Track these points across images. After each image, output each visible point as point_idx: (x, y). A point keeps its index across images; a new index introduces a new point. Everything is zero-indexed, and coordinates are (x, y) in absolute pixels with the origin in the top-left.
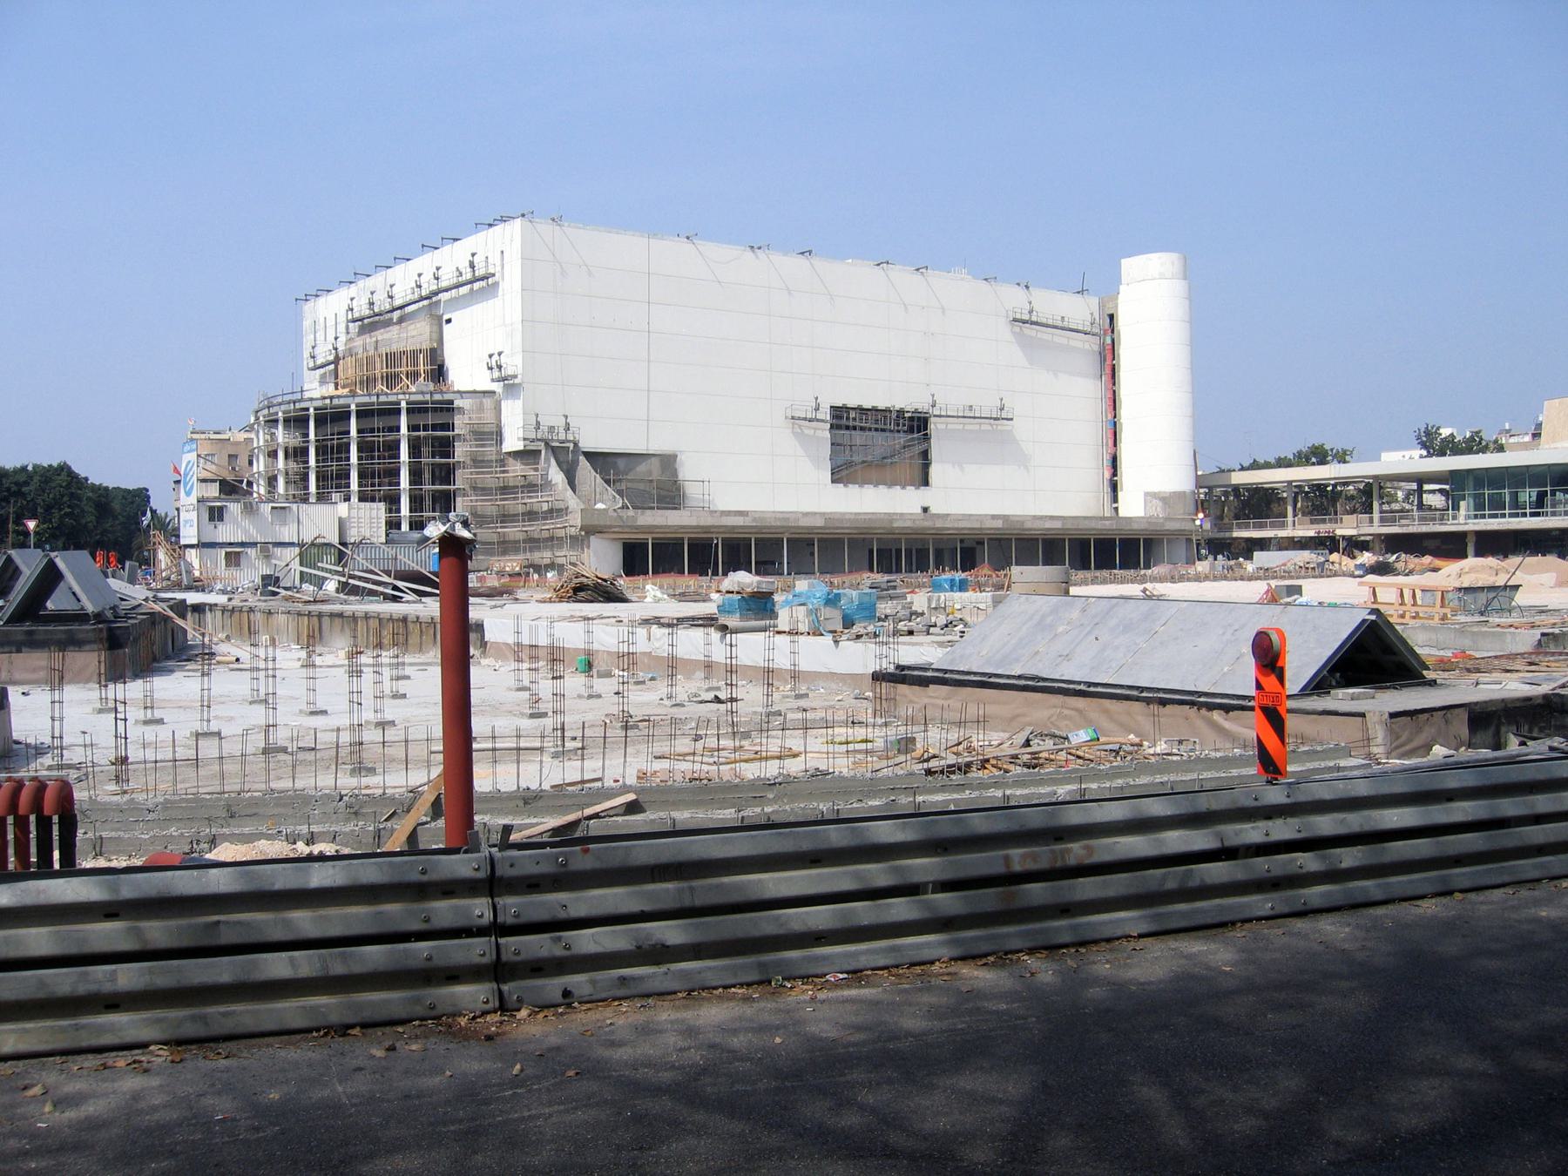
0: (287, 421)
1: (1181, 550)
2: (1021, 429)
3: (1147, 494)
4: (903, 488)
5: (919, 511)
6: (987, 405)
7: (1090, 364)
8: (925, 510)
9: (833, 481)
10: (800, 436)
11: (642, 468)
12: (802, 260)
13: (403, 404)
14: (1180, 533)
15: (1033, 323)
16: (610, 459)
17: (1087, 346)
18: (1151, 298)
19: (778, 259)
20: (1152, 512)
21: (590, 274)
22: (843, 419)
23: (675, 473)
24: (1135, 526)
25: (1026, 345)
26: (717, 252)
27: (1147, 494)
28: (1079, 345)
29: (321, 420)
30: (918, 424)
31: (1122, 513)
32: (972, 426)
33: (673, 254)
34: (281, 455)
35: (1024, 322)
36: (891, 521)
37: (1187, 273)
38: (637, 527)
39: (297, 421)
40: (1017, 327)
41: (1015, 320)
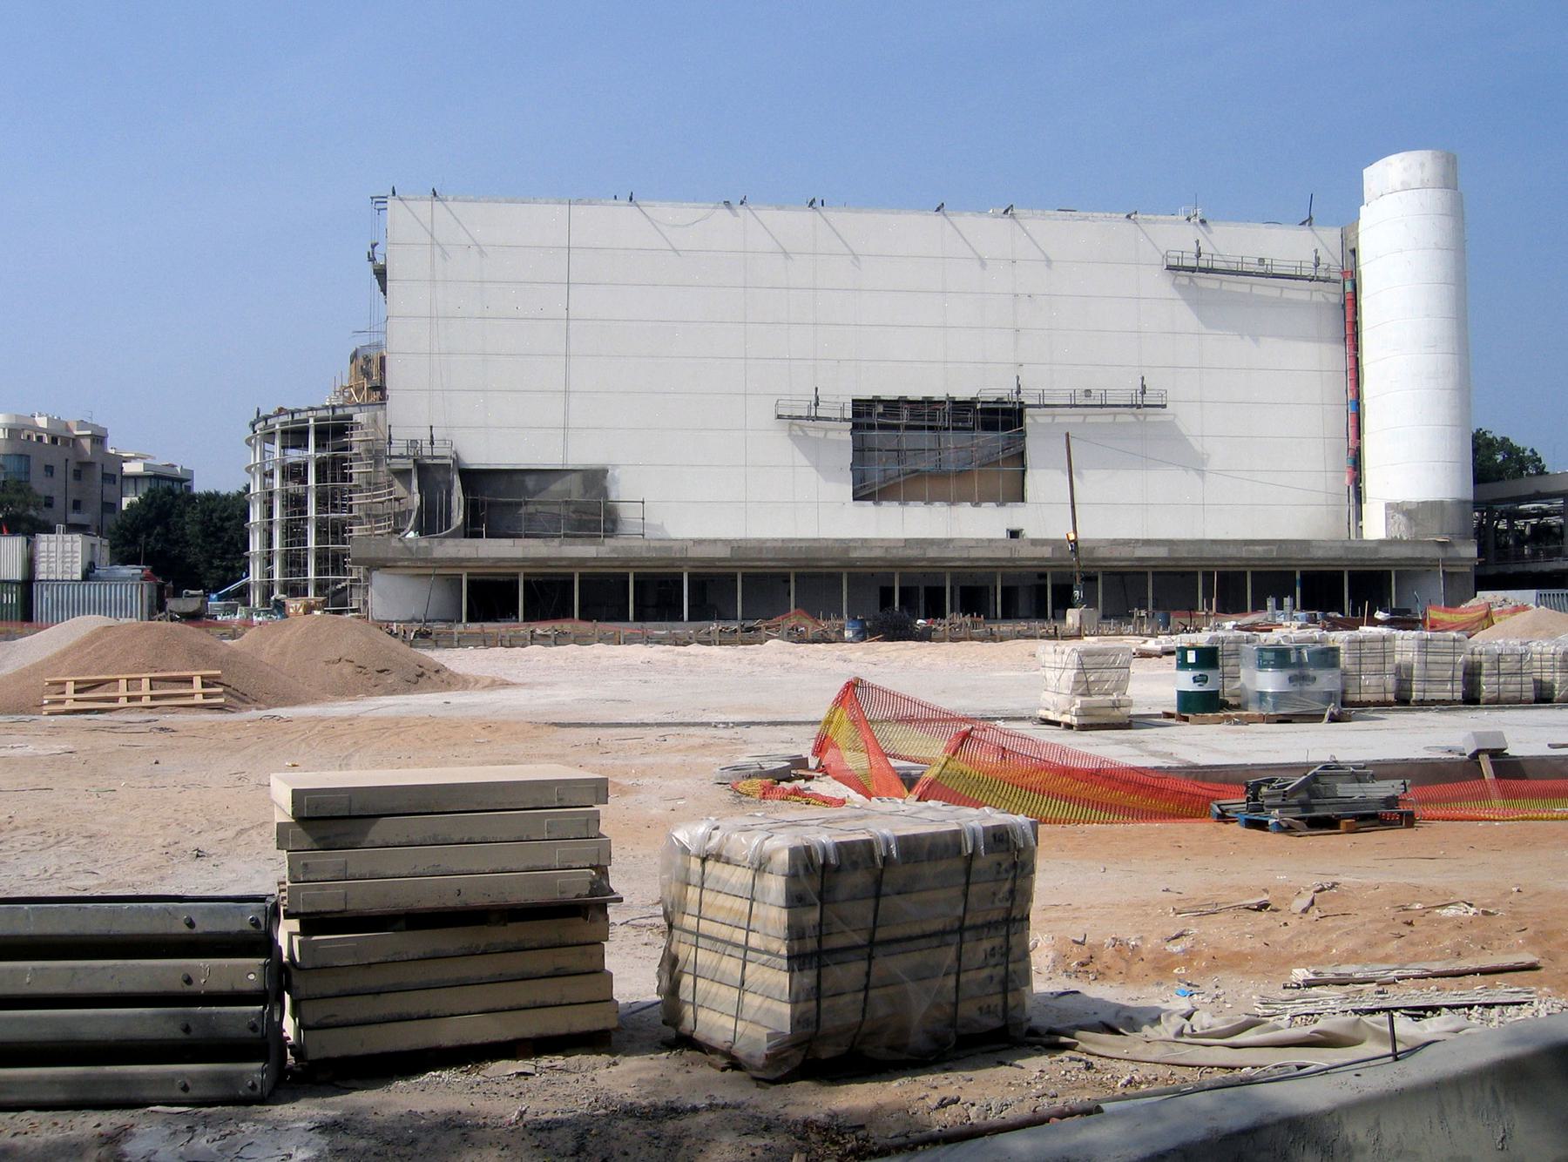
0: (284, 432)
1: (1437, 587)
2: (1186, 417)
3: (1389, 506)
4: (977, 505)
5: (1003, 535)
6: (1122, 386)
7: (1332, 324)
8: (1014, 534)
9: (858, 497)
10: (799, 441)
11: (557, 487)
12: (809, 215)
13: (311, 421)
14: (1434, 563)
15: (1202, 270)
16: (515, 478)
17: (1317, 297)
18: (1398, 218)
19: (769, 215)
20: (1396, 533)
21: (481, 253)
22: (872, 418)
23: (604, 492)
24: (1319, 554)
25: (1198, 302)
26: (666, 212)
27: (1389, 506)
28: (1304, 296)
29: (322, 433)
30: (1004, 418)
31: (1366, 537)
32: (1103, 417)
33: (607, 224)
34: (277, 475)
35: (1193, 270)
36: (847, 550)
37: (1451, 178)
38: (435, 560)
39: (295, 437)
40: (1183, 279)
41: (1169, 268)
